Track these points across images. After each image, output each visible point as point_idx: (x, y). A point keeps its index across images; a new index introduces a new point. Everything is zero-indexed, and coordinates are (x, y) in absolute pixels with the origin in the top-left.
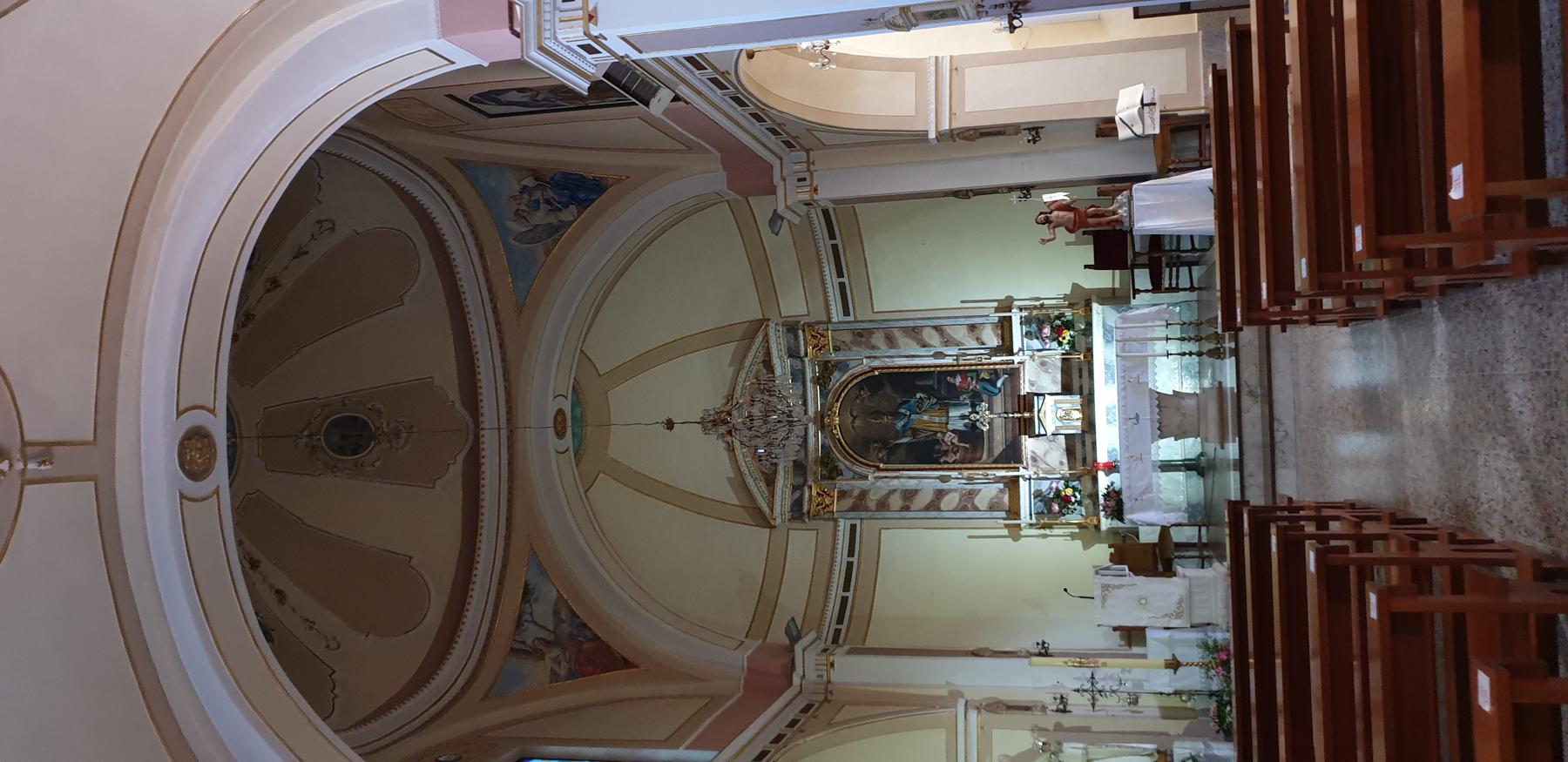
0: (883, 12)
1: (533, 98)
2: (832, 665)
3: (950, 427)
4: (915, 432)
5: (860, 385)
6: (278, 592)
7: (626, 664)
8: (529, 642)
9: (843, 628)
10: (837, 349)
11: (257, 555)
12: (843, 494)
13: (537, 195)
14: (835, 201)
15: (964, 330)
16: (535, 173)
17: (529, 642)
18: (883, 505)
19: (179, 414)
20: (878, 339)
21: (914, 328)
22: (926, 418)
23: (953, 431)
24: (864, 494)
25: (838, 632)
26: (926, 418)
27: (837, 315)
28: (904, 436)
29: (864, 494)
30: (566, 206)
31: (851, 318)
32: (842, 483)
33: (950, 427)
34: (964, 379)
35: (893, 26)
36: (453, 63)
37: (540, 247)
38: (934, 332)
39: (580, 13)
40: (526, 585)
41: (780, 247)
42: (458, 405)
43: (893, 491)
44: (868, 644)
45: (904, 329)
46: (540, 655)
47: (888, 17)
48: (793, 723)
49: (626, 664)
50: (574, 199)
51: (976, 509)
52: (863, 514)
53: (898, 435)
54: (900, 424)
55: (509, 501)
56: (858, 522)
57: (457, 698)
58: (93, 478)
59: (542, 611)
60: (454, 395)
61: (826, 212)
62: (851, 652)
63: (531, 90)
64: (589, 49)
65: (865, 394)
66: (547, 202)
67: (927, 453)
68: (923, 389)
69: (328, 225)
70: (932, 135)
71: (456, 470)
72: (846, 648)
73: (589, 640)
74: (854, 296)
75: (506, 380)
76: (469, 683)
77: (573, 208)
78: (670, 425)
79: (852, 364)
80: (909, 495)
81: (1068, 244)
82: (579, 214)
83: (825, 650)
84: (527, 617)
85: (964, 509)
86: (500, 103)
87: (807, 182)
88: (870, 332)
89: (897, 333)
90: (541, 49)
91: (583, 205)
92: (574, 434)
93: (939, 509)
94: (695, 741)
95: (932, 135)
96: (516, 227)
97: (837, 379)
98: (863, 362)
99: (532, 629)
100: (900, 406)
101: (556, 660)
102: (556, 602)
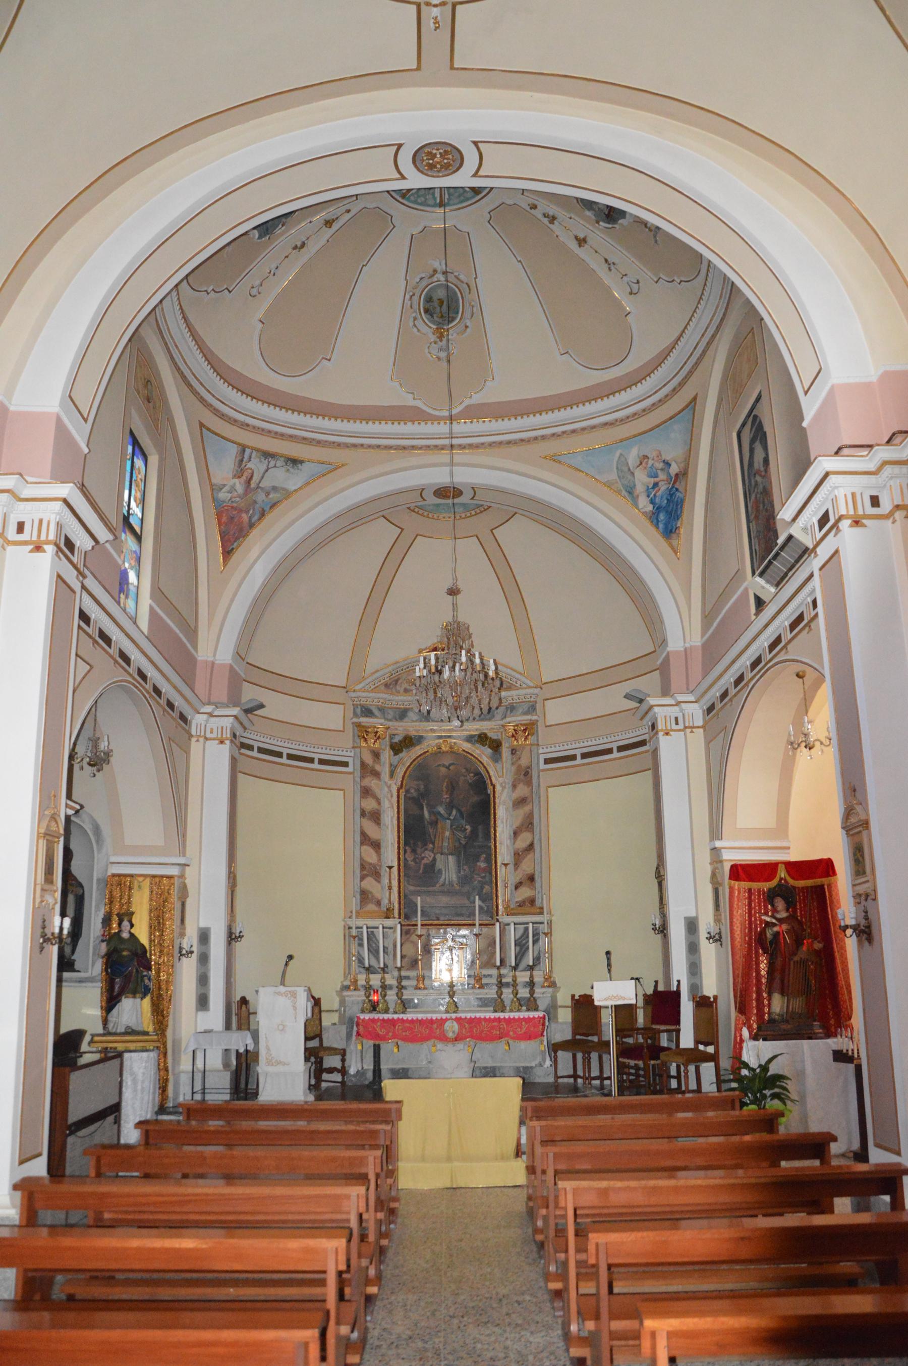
0: (864, 803)
1: (758, 472)
2: (222, 742)
3: (438, 856)
4: (434, 823)
5: (478, 774)
6: (303, 245)
7: (228, 553)
8: (250, 465)
9: (255, 753)
10: (513, 751)
11: (336, 226)
12: (376, 755)
13: (662, 476)
14: (655, 753)
15: (529, 871)
16: (682, 475)
17: (250, 465)
18: (366, 792)
19: (476, 143)
20: (522, 790)
21: (531, 824)
22: (447, 834)
23: (434, 860)
24: (377, 774)
25: (250, 748)
26: (447, 834)
27: (545, 752)
28: (430, 813)
29: (377, 774)
30: (652, 502)
31: (542, 766)
32: (387, 755)
33: (438, 856)
34: (484, 870)
35: (848, 812)
36: (806, 393)
37: (614, 476)
38: (528, 843)
39: (860, 512)
40: (301, 462)
41: (613, 700)
42: (467, 402)
43: (379, 802)
44: (240, 777)
45: (530, 815)
46: (238, 475)
47: (859, 809)
48: (171, 705)
49: (228, 553)
50: (658, 509)
51: (362, 878)
52: (358, 774)
53: (431, 807)
54: (441, 810)
55: (378, 447)
56: (350, 769)
57: (202, 400)
58: (419, 68)
59: (279, 476)
60: (477, 399)
61: (643, 743)
62: (234, 761)
63: (766, 471)
64: (824, 520)
65: (470, 777)
66: (656, 485)
67: (414, 833)
68: (474, 832)
69: (635, 287)
70: (718, 844)
71: (410, 401)
72: (237, 756)
73: (250, 518)
74: (561, 770)
75: (491, 445)
76: (216, 412)
77: (650, 508)
78: (453, 592)
79: (499, 766)
80: (376, 817)
81: (656, 982)
82: (644, 513)
83: (235, 736)
84: (272, 463)
85: (363, 867)
86: (752, 442)
87: (674, 727)
88: (529, 783)
89: (527, 809)
90: (827, 475)
91: (653, 518)
92: (438, 505)
93: (362, 843)
94: (157, 614)
95: (718, 844)
96: (633, 457)
97: (483, 754)
98: (501, 777)
99: (263, 467)
100: (459, 810)
101: (232, 489)
102: (284, 489)
